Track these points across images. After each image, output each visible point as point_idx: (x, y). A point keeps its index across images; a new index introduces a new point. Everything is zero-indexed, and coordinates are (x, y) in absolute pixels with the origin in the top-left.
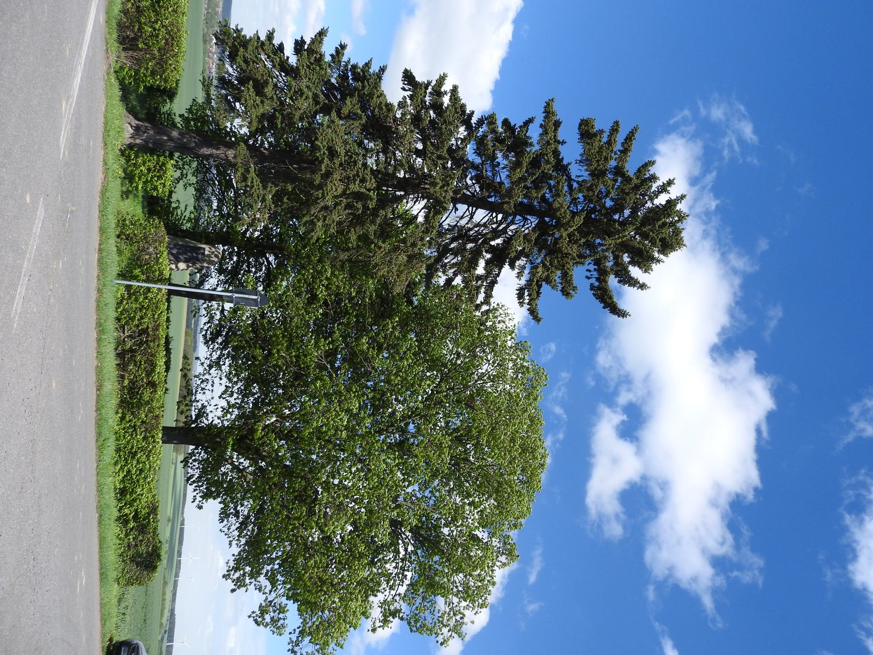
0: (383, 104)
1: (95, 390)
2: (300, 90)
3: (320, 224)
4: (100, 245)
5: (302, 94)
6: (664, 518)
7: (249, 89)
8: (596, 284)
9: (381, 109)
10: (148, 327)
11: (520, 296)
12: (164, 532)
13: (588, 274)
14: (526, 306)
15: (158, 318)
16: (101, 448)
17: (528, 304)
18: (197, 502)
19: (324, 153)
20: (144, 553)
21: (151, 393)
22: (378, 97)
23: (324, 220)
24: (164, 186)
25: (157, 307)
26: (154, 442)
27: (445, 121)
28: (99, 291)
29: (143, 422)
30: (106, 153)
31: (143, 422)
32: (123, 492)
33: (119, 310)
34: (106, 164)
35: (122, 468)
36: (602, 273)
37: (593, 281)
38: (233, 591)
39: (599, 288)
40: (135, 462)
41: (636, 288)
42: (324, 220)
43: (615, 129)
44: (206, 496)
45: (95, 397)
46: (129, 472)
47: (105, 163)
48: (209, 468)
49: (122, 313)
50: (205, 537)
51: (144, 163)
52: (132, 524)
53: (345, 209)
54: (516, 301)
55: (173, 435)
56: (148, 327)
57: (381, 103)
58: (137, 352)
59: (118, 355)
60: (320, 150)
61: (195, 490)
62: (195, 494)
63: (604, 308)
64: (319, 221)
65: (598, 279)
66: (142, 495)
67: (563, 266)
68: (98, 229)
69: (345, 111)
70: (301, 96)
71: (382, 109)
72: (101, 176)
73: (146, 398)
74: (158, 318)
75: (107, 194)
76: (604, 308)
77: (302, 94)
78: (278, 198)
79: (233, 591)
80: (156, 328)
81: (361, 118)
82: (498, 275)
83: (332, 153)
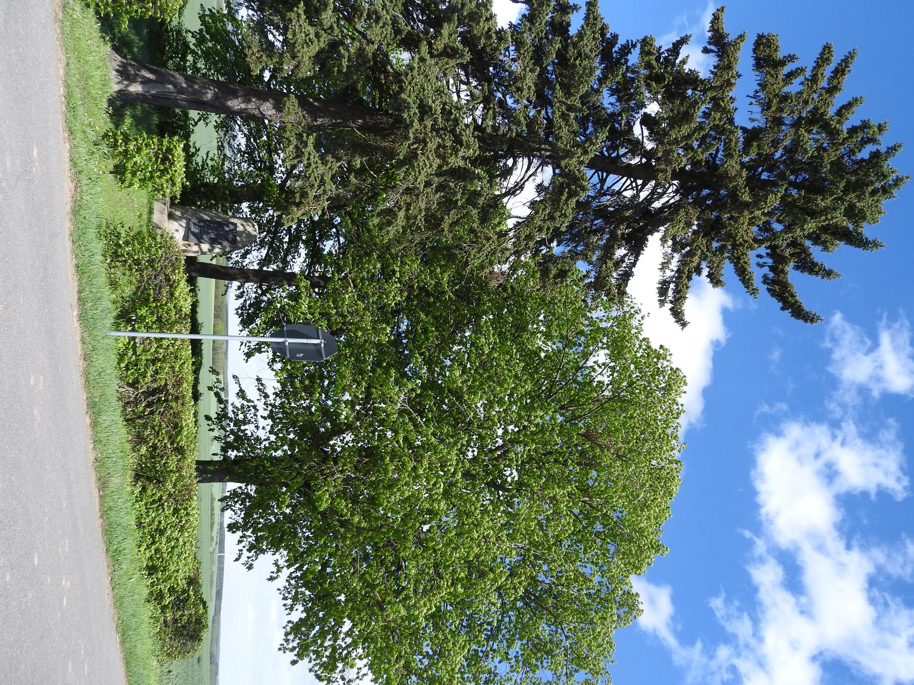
0: (493, 30)
1: (96, 491)
2: (376, 12)
3: (401, 214)
4: (80, 292)
5: (378, 18)
6: (763, 511)
7: (299, 15)
8: (771, 275)
9: (488, 37)
10: (166, 385)
11: (663, 291)
12: (208, 593)
13: (761, 261)
14: (669, 306)
15: (180, 371)
16: (114, 555)
17: (671, 302)
18: (244, 559)
19: (415, 114)
20: (186, 621)
21: (179, 461)
22: (487, 20)
23: (408, 209)
24: (174, 184)
25: (176, 357)
26: (188, 514)
27: (579, 54)
28: (86, 357)
29: (170, 495)
30: (74, 148)
31: (170, 495)
32: (152, 570)
33: (123, 365)
34: (75, 165)
35: (148, 547)
36: (778, 260)
37: (766, 270)
38: (294, 663)
39: (774, 282)
40: (164, 540)
41: (819, 277)
42: (408, 209)
43: (824, 58)
44: (256, 548)
45: (97, 500)
46: (157, 550)
47: (73, 163)
48: (254, 508)
49: (127, 369)
50: (253, 597)
51: (139, 150)
52: (167, 601)
53: (436, 192)
54: (656, 297)
55: (209, 471)
56: (166, 385)
57: (490, 30)
58: (151, 404)
59: (129, 421)
60: (408, 108)
61: (240, 542)
62: (240, 546)
63: (783, 309)
64: (400, 209)
65: (772, 269)
66: (177, 571)
67: (739, 258)
68: (71, 270)
69: (439, 45)
70: (377, 22)
71: (491, 37)
72: (68, 186)
73: (172, 466)
74: (180, 371)
75: (82, 212)
76: (783, 309)
77: (378, 18)
78: (341, 178)
79: (294, 663)
80: (178, 384)
81: (462, 56)
82: (634, 264)
83: (424, 110)
